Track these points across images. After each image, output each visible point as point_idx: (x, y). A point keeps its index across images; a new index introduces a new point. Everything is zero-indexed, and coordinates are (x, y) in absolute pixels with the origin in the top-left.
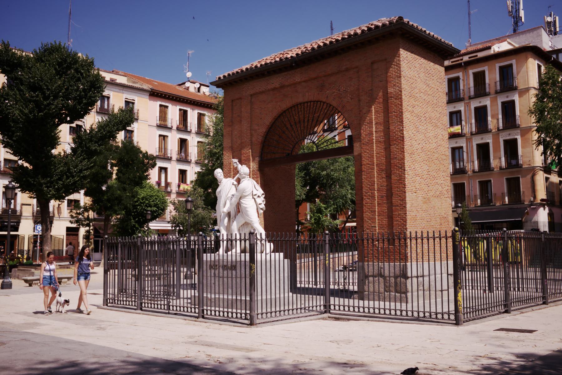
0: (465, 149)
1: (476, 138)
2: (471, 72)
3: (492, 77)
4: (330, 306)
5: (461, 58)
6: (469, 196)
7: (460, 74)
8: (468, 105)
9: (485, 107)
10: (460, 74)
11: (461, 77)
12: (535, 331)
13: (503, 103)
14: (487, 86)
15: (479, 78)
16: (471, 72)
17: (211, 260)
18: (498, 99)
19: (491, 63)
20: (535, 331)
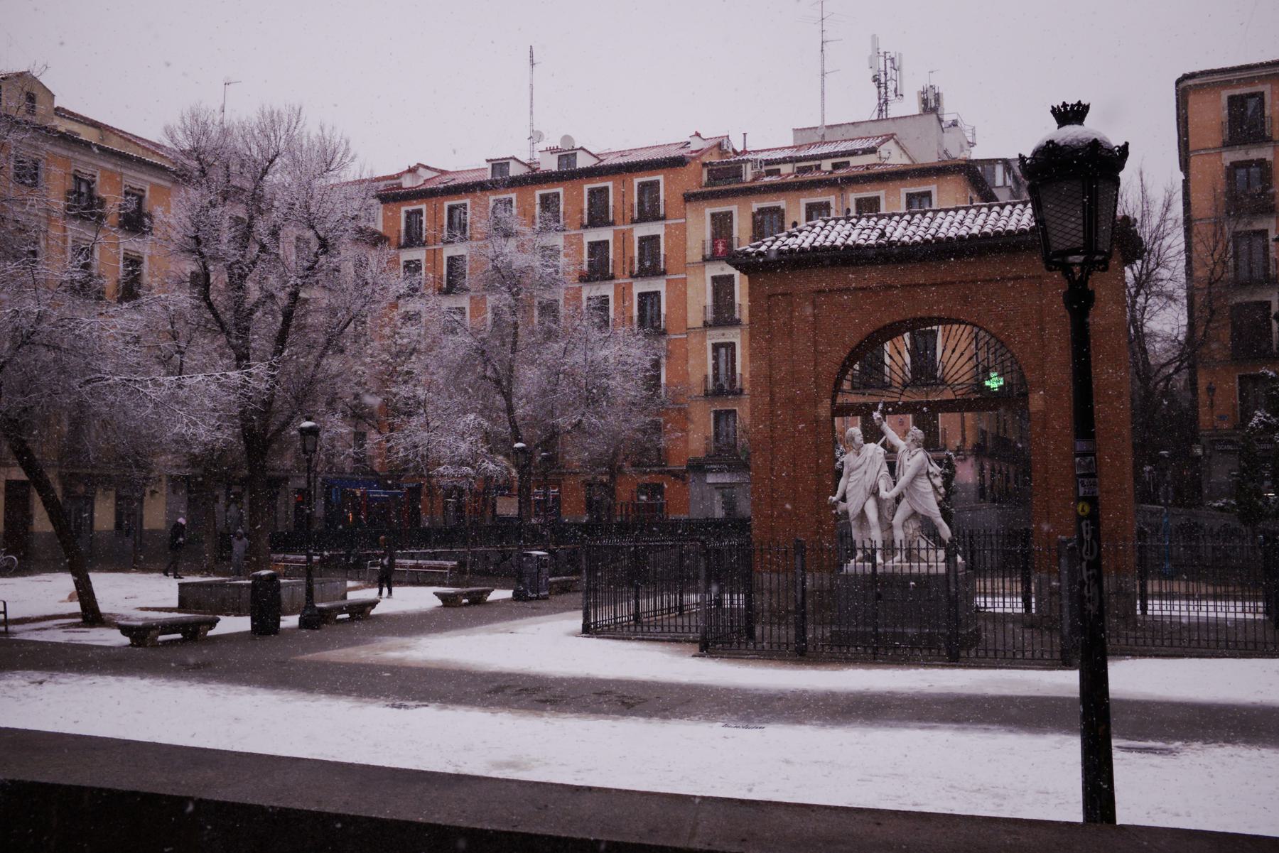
5: (817, 162)
10: (832, 199)
11: (833, 205)
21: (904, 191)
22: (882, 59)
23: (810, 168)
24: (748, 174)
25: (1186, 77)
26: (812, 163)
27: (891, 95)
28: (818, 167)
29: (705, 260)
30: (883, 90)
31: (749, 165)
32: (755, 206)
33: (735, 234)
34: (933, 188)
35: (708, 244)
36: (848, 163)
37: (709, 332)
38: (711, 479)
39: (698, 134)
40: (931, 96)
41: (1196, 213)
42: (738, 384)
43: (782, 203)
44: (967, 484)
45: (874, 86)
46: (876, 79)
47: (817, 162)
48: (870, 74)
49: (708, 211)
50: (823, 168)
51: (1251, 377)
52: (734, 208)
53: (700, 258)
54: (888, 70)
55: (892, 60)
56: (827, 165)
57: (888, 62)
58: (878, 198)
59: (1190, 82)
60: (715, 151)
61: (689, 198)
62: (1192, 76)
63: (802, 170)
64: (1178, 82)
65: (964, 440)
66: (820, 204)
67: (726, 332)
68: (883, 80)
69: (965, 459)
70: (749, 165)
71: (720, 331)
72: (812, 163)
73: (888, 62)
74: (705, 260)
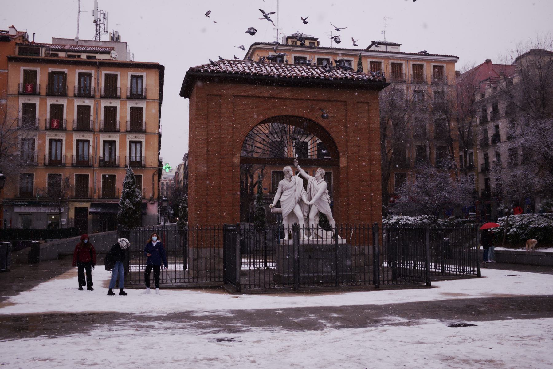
0: (91, 143)
1: (104, 135)
2: (104, 72)
3: (98, 81)
4: (379, 281)
5: (79, 54)
7: (93, 72)
8: (97, 104)
9: (115, 108)
10: (93, 72)
11: (93, 74)
12: (485, 277)
13: (132, 108)
14: (118, 89)
15: (30, 77)
16: (104, 72)
17: (219, 248)
18: (128, 104)
19: (124, 70)
20: (485, 277)
21: (130, 74)
22: (99, 13)
23: (74, 56)
24: (43, 53)
25: (256, 44)
26: (76, 54)
27: (102, 31)
28: (79, 56)
29: (19, 94)
30: (98, 28)
31: (44, 49)
32: (50, 70)
33: (38, 82)
34: (144, 74)
35: (22, 85)
36: (95, 57)
37: (47, 133)
38: (17, 210)
39: (13, 27)
40: (116, 36)
41: (157, 105)
42: (36, 161)
43: (66, 71)
44: (154, 215)
45: (94, 25)
46: (95, 22)
47: (79, 54)
48: (93, 19)
49: (22, 68)
50: (82, 57)
51: (277, 172)
52: (38, 69)
53: (16, 93)
54: (102, 19)
55: (104, 14)
56: (84, 56)
57: (102, 15)
58: (117, 75)
59: (258, 46)
60: (21, 38)
61: (11, 59)
62: (259, 44)
63: (69, 56)
64: (252, 45)
65: (153, 194)
66: (87, 73)
67: (58, 133)
68: (99, 23)
69: (154, 204)
70: (44, 49)
71: (134, 135)
72: (76, 54)
73: (102, 15)
74: (19, 94)
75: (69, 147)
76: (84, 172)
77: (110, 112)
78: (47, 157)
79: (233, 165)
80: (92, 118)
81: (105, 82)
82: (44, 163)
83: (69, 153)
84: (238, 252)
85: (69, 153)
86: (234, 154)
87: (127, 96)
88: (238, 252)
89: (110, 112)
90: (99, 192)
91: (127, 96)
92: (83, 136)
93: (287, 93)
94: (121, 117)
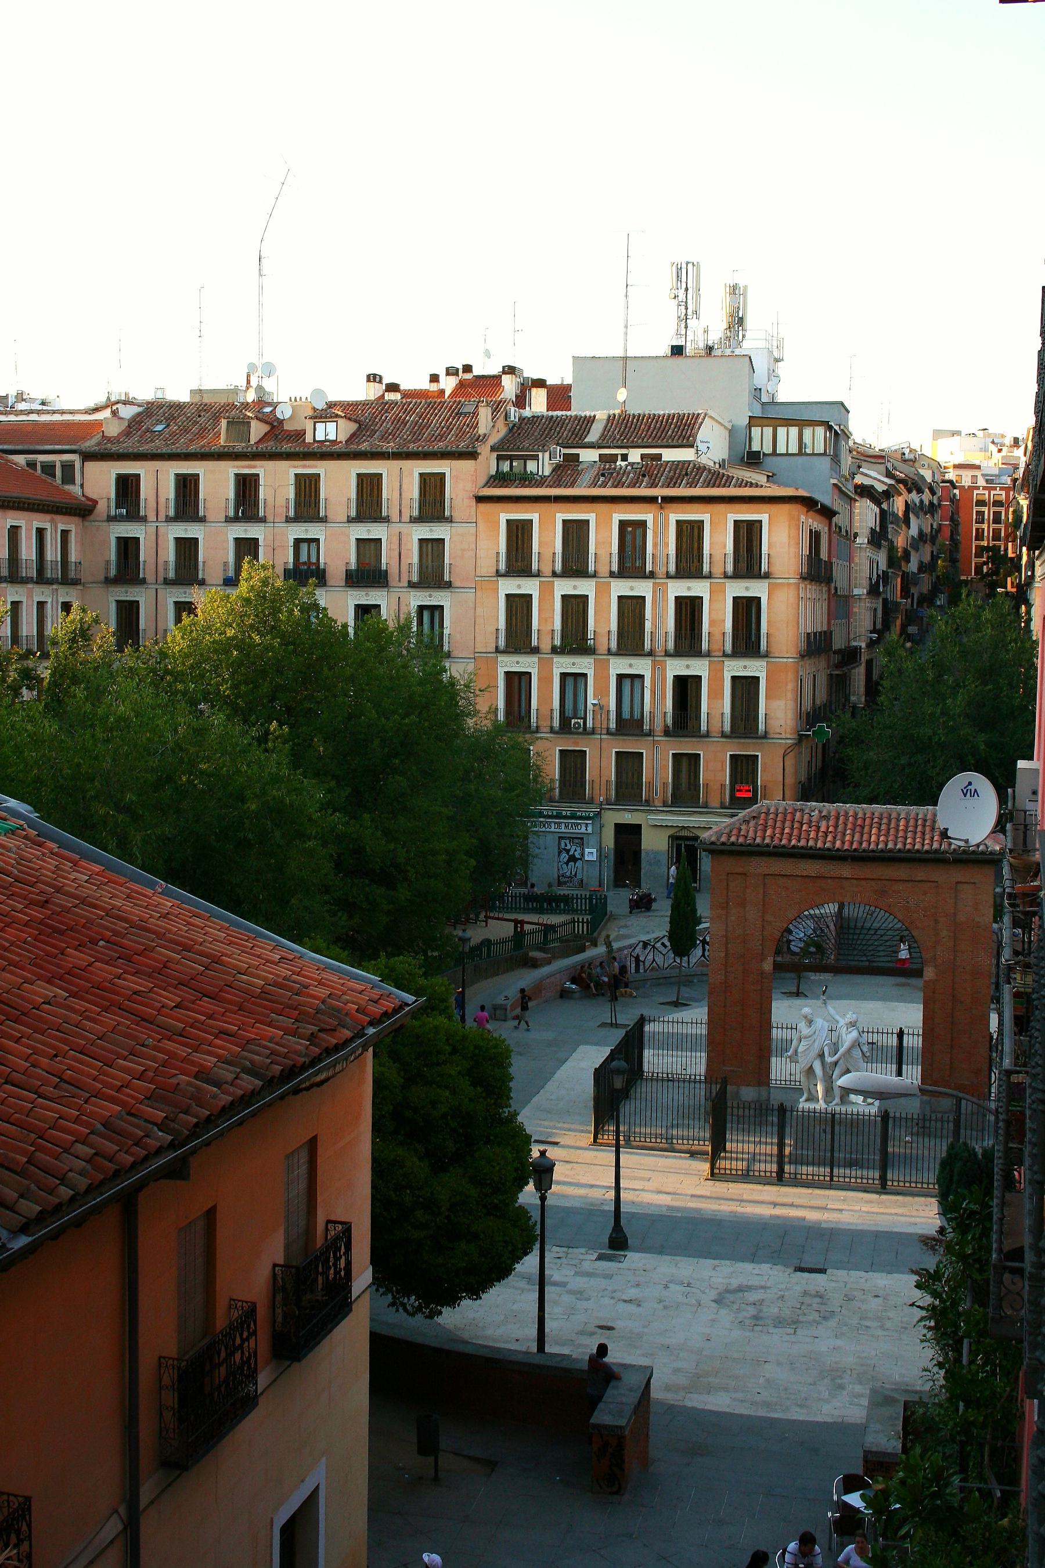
0: (647, 682)
5: (624, 451)
6: (650, 784)
28: (625, 457)
36: (659, 457)
50: (630, 459)
75: (602, 690)
76: (630, 746)
77: (689, 610)
78: (556, 715)
79: (762, 973)
80: (648, 625)
81: (677, 539)
82: (552, 727)
83: (600, 697)
84: (1041, 771)
85: (600, 697)
86: (763, 958)
87: (666, 726)
88: (1041, 771)
89: (689, 610)
90: (665, 792)
91: (666, 726)
92: (631, 666)
93: (846, 870)
94: (712, 623)
